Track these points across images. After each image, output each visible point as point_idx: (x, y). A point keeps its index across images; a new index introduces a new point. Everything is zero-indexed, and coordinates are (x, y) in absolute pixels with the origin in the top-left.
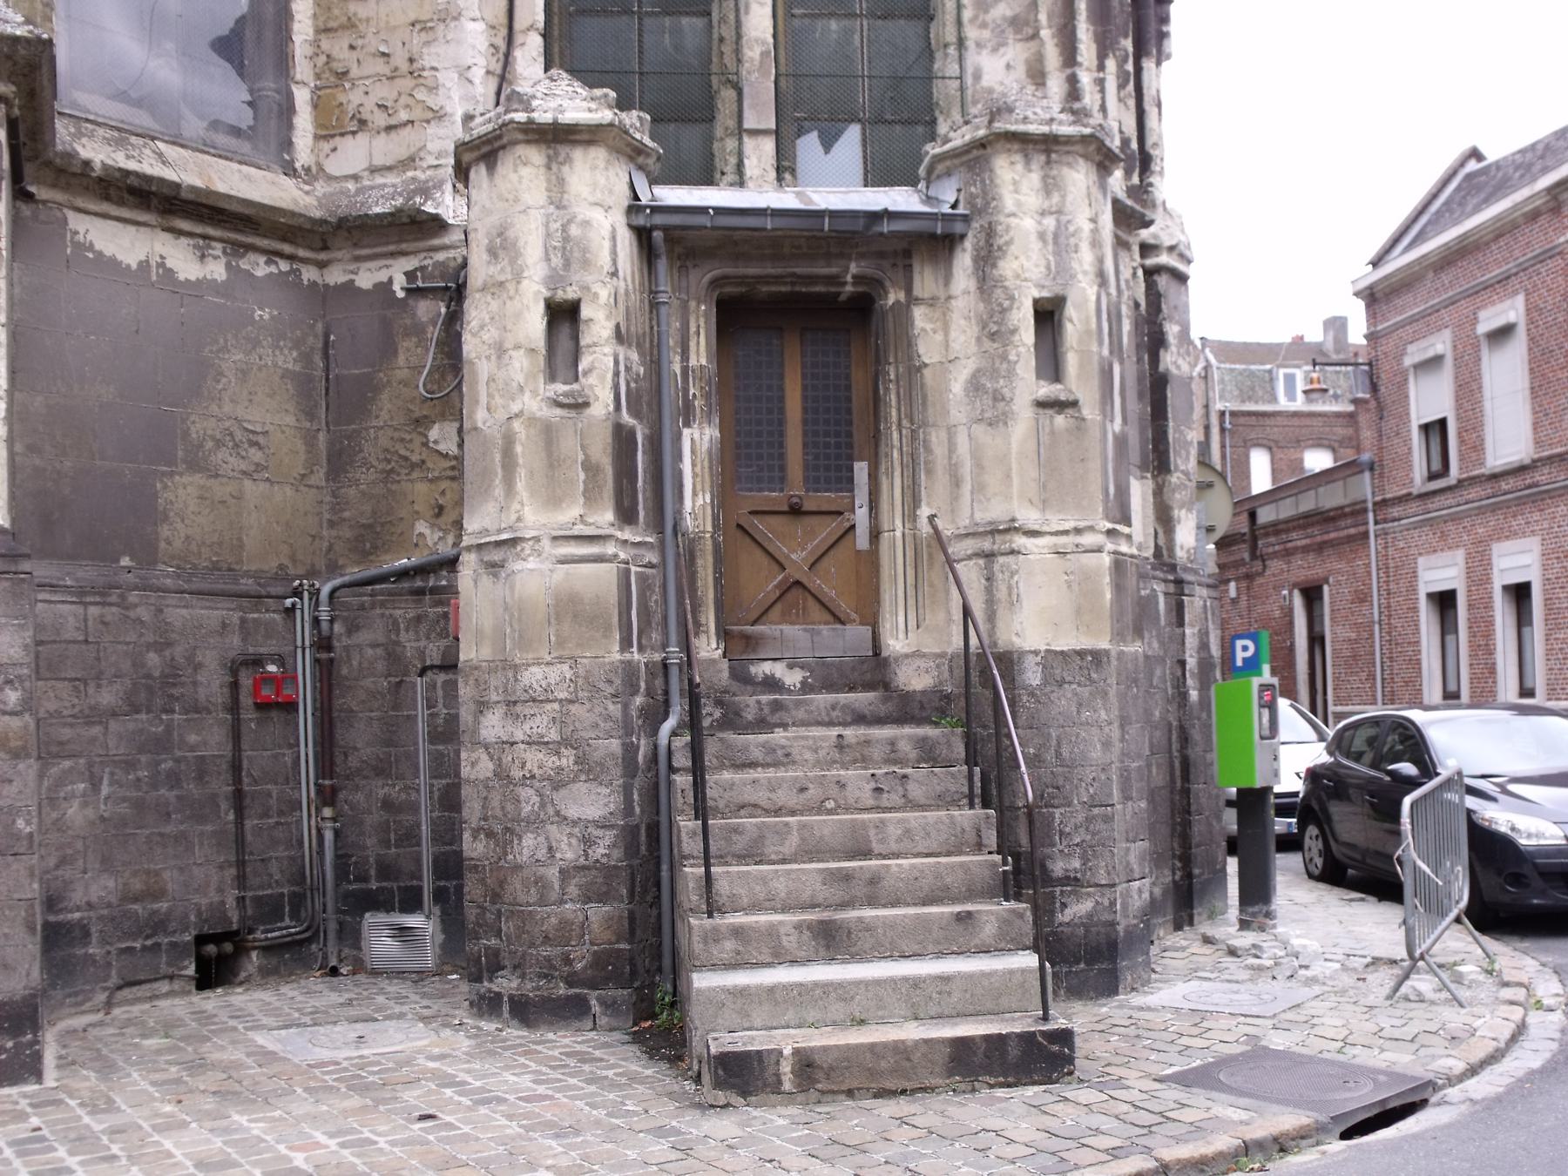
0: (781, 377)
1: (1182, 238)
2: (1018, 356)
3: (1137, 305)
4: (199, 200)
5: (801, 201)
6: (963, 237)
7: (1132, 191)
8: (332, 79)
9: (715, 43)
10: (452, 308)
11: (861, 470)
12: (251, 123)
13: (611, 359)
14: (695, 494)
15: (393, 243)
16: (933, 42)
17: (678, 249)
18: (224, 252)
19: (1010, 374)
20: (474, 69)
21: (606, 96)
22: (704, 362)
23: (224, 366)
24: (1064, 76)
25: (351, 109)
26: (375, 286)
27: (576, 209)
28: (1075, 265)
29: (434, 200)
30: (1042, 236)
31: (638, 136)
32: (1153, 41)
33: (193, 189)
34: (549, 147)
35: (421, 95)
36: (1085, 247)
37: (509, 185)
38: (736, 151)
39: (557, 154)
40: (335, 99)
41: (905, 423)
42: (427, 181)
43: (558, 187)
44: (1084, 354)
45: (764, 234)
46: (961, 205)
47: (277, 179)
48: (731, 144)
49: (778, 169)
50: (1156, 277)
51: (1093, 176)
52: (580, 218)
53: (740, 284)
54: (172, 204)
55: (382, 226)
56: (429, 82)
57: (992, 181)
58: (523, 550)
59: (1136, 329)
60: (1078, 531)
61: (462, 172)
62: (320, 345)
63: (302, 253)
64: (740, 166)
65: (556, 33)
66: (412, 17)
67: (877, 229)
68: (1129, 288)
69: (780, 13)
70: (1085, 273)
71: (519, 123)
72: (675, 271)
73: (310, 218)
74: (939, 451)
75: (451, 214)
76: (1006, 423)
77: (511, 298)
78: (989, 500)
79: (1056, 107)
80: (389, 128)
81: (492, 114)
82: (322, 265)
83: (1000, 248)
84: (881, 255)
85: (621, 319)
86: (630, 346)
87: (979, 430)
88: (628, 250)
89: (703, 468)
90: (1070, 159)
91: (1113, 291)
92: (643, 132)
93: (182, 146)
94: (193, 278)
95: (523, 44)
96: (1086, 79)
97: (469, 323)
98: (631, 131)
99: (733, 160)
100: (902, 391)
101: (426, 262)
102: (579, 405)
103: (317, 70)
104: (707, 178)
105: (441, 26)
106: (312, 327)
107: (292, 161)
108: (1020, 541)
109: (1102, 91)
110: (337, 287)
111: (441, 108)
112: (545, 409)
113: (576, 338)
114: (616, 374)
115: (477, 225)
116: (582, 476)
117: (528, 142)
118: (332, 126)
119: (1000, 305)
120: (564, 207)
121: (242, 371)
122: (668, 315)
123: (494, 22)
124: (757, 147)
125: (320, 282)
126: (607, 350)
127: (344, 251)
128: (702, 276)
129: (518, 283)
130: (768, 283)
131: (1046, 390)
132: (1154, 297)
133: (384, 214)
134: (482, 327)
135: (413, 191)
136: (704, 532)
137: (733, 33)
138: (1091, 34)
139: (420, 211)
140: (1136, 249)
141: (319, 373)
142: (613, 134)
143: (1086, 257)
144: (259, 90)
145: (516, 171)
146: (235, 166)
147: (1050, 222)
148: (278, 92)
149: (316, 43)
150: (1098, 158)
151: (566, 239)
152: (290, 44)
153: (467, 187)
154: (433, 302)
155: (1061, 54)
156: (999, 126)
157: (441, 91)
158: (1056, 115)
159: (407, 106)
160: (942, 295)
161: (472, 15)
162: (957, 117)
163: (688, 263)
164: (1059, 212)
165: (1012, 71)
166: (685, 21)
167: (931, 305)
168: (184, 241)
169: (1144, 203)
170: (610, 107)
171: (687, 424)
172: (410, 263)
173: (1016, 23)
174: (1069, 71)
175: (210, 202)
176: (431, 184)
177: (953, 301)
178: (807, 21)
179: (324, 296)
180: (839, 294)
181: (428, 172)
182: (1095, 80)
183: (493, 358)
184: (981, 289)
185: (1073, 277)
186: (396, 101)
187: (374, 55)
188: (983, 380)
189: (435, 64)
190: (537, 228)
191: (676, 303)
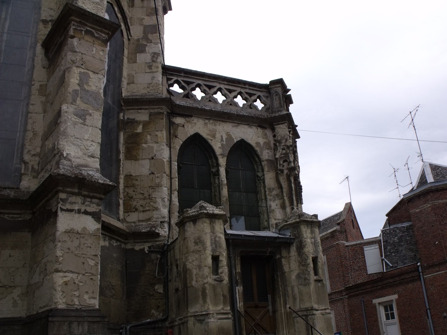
6: (293, 243)
8: (128, 198)
11: (269, 297)
14: (239, 303)
16: (258, 199)
18: (108, 239)
19: (309, 274)
20: (165, 198)
30: (312, 243)
35: (152, 204)
39: (212, 221)
41: (282, 285)
43: (213, 229)
46: (292, 236)
57: (300, 231)
58: (210, 316)
60: (325, 309)
66: (150, 185)
70: (321, 251)
74: (290, 292)
76: (309, 285)
78: (305, 303)
80: (143, 211)
83: (304, 246)
87: (301, 287)
89: (241, 296)
101: (154, 244)
102: (221, 281)
103: (124, 196)
105: (157, 188)
107: (119, 218)
108: (315, 312)
111: (157, 207)
112: (213, 281)
116: (222, 298)
117: (206, 217)
118: (128, 209)
119: (305, 258)
120: (214, 233)
125: (125, 247)
129: (205, 251)
131: (315, 278)
133: (145, 232)
134: (193, 261)
136: (242, 312)
139: (154, 232)
149: (124, 189)
151: (215, 241)
152: (119, 189)
155: (290, 203)
157: (157, 203)
159: (148, 206)
161: (165, 186)
171: (237, 286)
172: (149, 244)
173: (277, 195)
179: (126, 251)
181: (154, 222)
186: (145, 205)
188: (301, 275)
189: (156, 197)
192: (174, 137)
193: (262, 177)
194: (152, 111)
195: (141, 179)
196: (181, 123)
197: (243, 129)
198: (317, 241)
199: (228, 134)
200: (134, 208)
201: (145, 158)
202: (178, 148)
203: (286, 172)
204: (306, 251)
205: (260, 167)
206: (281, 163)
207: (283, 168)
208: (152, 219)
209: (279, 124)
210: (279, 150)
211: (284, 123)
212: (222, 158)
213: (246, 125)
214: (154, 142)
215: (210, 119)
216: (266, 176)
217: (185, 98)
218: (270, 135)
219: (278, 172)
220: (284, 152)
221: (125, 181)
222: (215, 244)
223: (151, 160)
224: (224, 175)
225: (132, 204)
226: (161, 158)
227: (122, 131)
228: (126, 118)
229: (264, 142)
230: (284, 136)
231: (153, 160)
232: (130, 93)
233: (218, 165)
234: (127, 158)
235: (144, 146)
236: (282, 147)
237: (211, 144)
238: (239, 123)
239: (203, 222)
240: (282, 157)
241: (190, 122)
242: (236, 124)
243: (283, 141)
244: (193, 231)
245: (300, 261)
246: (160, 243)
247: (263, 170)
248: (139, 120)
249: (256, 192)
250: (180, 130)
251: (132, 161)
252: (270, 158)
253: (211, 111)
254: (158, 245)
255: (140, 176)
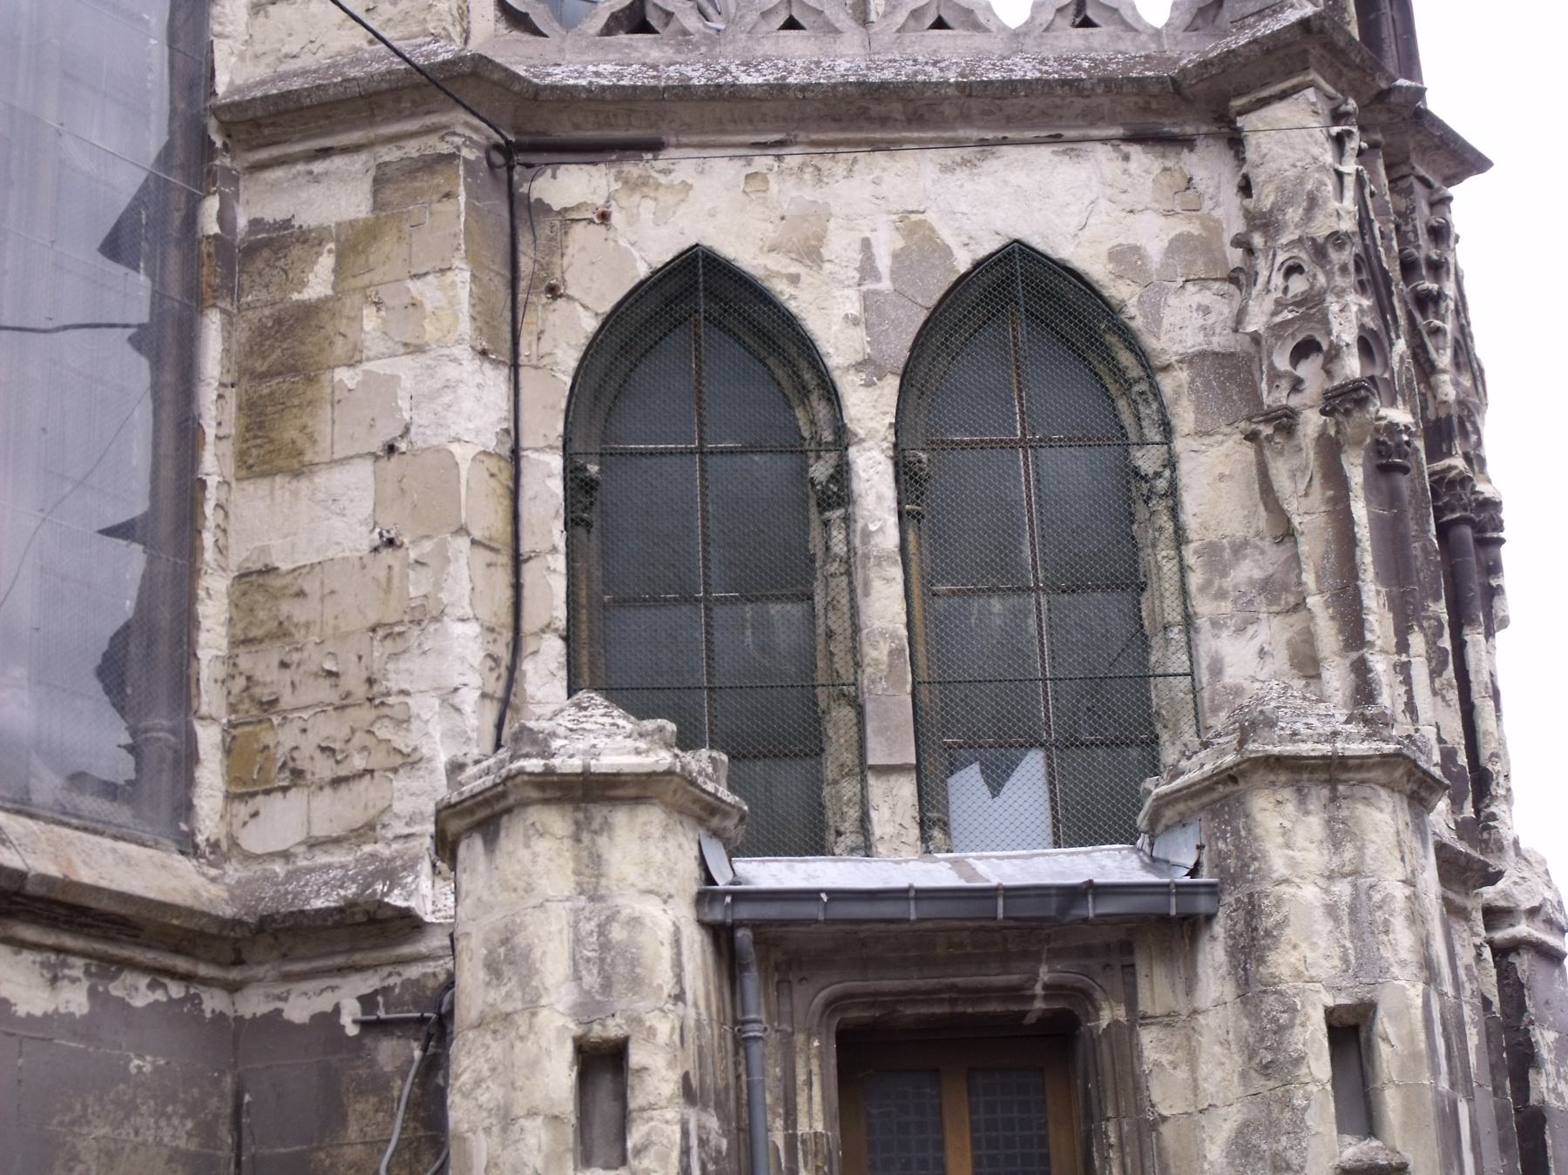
0: (940, 1145)
1: (1549, 895)
2: (1308, 1099)
3: (1487, 1003)
4: (52, 895)
5: (961, 876)
6: (1210, 918)
7: (1464, 829)
8: (254, 712)
9: (821, 640)
10: (431, 1050)
12: (132, 776)
13: (677, 1128)
15: (340, 953)
16: (1146, 623)
17: (777, 955)
18: (87, 972)
19: (1297, 1128)
20: (463, 691)
21: (661, 729)
22: (819, 1127)
23: (81, 1145)
24: (1348, 662)
25: (281, 754)
26: (314, 1017)
27: (620, 901)
28: (1386, 953)
29: (404, 887)
30: (1331, 910)
31: (710, 787)
32: (1478, 602)
33: (45, 879)
34: (577, 809)
36: (1399, 924)
37: (518, 868)
38: (857, 799)
39: (589, 819)
40: (258, 741)
42: (393, 859)
44: (1411, 1092)
45: (906, 926)
46: (1205, 870)
47: (168, 861)
48: (849, 788)
49: (922, 824)
50: (1512, 958)
51: (1405, 816)
52: (625, 913)
53: (872, 1005)
54: (12, 903)
55: (326, 928)
56: (397, 713)
57: (1249, 831)
59: (1488, 1041)
61: (446, 848)
62: (228, 1110)
63: (203, 970)
64: (864, 821)
65: (584, 635)
66: (373, 619)
67: (1078, 912)
68: (1471, 978)
69: (916, 591)
70: (1403, 964)
71: (531, 774)
72: (772, 989)
73: (217, 917)
75: (430, 908)
77: (522, 1038)
79: (1341, 715)
80: (337, 782)
81: (492, 761)
82: (233, 988)
83: (1268, 933)
84: (1086, 951)
85: (691, 1066)
86: (705, 1107)
88: (699, 959)
90: (1367, 792)
91: (1448, 988)
92: (717, 781)
93: (31, 816)
94: (38, 1012)
95: (535, 653)
96: (1380, 665)
97: (457, 1077)
98: (700, 780)
99: (853, 813)
100: (1128, 1160)
101: (391, 981)
103: (232, 700)
104: (815, 843)
105: (416, 631)
106: (216, 1082)
107: (192, 834)
109: (1407, 681)
110: (254, 1020)
111: (415, 749)
113: (622, 1097)
114: (685, 1152)
115: (470, 927)
117: (546, 802)
119: (1275, 1020)
120: (601, 898)
121: (109, 1154)
122: (763, 1055)
123: (493, 622)
124: (889, 793)
125: (230, 1013)
126: (671, 1114)
127: (267, 967)
128: (812, 996)
129: (534, 1014)
130: (914, 1002)
132: (1513, 990)
133: (328, 909)
134: (478, 1083)
135: (372, 874)
137: (847, 624)
138: (1383, 599)
139: (381, 904)
140: (1478, 916)
141: (226, 1153)
142: (672, 786)
143: (1403, 939)
144: (146, 731)
145: (527, 846)
146: (108, 843)
147: (1343, 889)
148: (173, 732)
149: (231, 660)
150: (1409, 787)
151: (605, 946)
152: (194, 663)
153: (453, 868)
154: (402, 1041)
156: (1255, 748)
157: (415, 725)
158: (1339, 728)
159: (364, 748)
160: (1183, 1007)
161: (460, 613)
162: (1189, 735)
163: (791, 977)
164: (1356, 873)
165: (1269, 660)
166: (775, 609)
167: (1168, 1025)
168: (28, 956)
169: (1484, 846)
170: (668, 746)
172: (367, 983)
173: (1268, 587)
174: (1354, 655)
175: (69, 898)
176: (399, 863)
177: (1200, 1017)
178: (955, 601)
180: (1024, 1014)
181: (395, 846)
182: (1395, 666)
183: (495, 1130)
184: (1242, 997)
185: (1384, 971)
186: (348, 741)
187: (316, 675)
188: (1255, 1139)
189: (405, 686)
190: (561, 931)
191: (774, 1037)
192: (544, 299)
193: (1158, 475)
194: (390, 154)
195: (322, 583)
196: (589, 199)
197: (1017, 177)
198: (1377, 897)
199: (914, 228)
200: (284, 764)
201: (351, 453)
202: (568, 359)
203: (1312, 423)
204: (1284, 971)
205: (1149, 411)
206: (1282, 362)
207: (1295, 401)
208: (384, 826)
209: (1264, 102)
210: (1261, 280)
211: (1296, 89)
212: (868, 384)
213: (1037, 142)
214: (402, 350)
215: (781, 144)
216: (1184, 467)
217: (623, 38)
218: (1218, 188)
219: (1261, 427)
220: (1298, 285)
221: (237, 606)
222: (601, 970)
223: (383, 463)
224: (880, 498)
225: (272, 745)
226: (443, 440)
227: (214, 306)
228: (242, 222)
229: (1171, 242)
230: (1300, 181)
231: (395, 458)
232: (268, 65)
233: (842, 438)
234: (250, 467)
235: (341, 381)
236: (1281, 258)
237: (793, 306)
238: (989, 135)
239: (531, 832)
240: (1285, 324)
241: (645, 184)
242: (967, 152)
243: (1293, 214)
244: (486, 896)
245: (1251, 1040)
246: (429, 970)
247: (1167, 429)
248: (313, 223)
249: (1133, 582)
250: (582, 249)
251: (278, 479)
252: (1215, 339)
253: (779, 90)
254: (418, 981)
255: (318, 568)
